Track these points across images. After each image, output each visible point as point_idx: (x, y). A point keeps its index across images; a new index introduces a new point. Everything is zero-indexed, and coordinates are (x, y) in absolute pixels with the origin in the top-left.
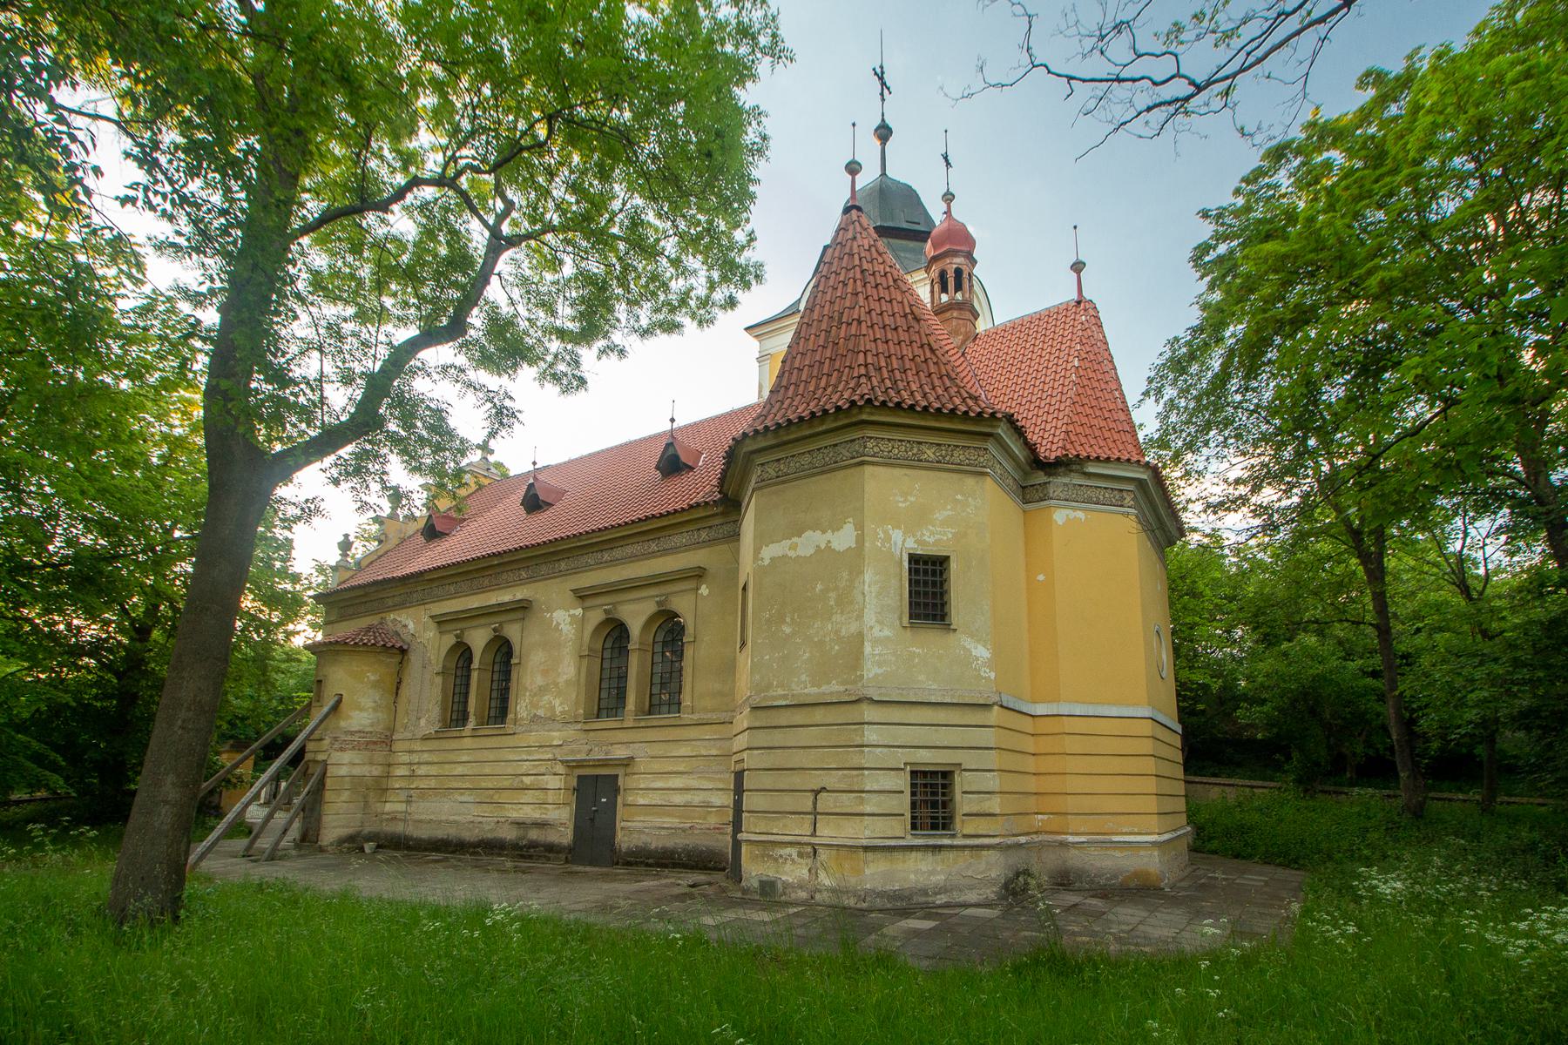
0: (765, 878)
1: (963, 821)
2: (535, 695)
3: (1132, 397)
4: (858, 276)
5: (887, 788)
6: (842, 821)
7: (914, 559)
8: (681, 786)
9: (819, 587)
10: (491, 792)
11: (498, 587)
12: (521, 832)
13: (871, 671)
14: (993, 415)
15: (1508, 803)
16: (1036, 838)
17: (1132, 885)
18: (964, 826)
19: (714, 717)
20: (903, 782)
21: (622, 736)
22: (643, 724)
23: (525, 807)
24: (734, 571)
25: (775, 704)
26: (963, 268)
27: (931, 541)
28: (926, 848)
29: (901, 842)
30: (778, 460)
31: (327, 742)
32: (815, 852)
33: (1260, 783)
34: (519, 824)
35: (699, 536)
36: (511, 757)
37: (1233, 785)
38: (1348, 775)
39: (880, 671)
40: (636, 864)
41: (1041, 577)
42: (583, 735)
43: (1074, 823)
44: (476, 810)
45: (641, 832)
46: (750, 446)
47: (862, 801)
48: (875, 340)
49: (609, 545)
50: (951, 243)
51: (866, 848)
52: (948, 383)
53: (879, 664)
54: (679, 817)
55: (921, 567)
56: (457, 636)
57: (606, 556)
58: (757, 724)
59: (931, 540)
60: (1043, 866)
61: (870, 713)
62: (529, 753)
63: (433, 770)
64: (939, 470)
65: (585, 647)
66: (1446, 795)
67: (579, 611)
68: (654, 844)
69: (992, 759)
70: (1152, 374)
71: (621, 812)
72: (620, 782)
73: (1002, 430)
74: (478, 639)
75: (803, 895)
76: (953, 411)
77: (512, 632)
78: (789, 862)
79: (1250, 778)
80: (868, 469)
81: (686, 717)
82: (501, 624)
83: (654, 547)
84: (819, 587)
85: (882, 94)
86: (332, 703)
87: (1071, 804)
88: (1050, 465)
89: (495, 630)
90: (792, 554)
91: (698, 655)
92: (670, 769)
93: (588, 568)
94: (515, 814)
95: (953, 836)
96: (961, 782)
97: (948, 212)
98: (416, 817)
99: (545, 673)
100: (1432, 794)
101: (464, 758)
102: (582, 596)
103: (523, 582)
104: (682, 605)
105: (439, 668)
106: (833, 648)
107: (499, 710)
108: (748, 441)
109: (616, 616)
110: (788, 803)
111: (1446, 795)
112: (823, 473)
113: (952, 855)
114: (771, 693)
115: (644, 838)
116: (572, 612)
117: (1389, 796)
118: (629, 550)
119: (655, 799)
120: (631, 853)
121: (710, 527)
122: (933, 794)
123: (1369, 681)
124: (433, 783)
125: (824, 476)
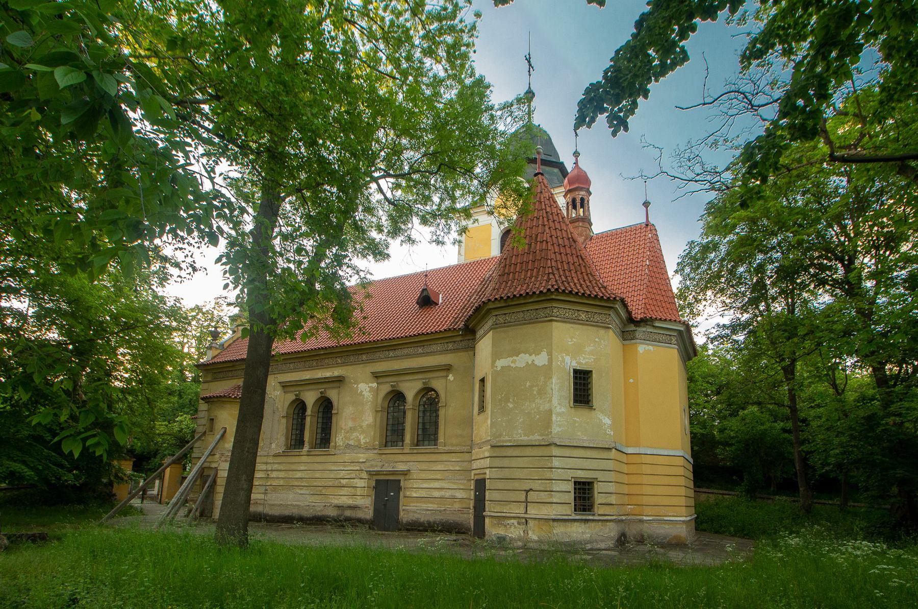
1: (598, 508)
2: (348, 432)
3: (670, 273)
4: (545, 215)
5: (564, 490)
6: (541, 506)
7: (576, 371)
9: (528, 384)
10: (320, 488)
12: (340, 512)
13: (555, 429)
14: (615, 298)
15: (854, 506)
16: (629, 518)
17: (673, 542)
18: (599, 510)
19: (458, 449)
20: (570, 487)
21: (402, 457)
22: (415, 451)
23: (342, 497)
24: (471, 367)
25: (505, 444)
26: (585, 197)
27: (584, 363)
28: (582, 520)
29: (570, 517)
30: (505, 314)
31: (217, 456)
32: (527, 521)
33: (727, 492)
34: (338, 507)
35: (448, 346)
37: (713, 493)
38: (772, 489)
39: (560, 430)
40: (412, 530)
41: (631, 381)
42: (377, 456)
43: (647, 510)
44: (313, 499)
46: (491, 306)
47: (551, 496)
48: (555, 253)
49: (394, 347)
50: (579, 183)
51: (554, 520)
52: (591, 279)
53: (560, 426)
54: (437, 504)
55: (578, 375)
56: (296, 395)
57: (391, 354)
58: (494, 455)
59: (584, 362)
60: (632, 531)
61: (555, 451)
63: (282, 475)
64: (587, 325)
65: (379, 406)
66: (823, 501)
67: (375, 385)
68: (423, 519)
69: (612, 476)
70: (680, 260)
71: (402, 500)
72: (402, 484)
73: (618, 306)
74: (310, 398)
75: (520, 544)
76: (596, 296)
77: (333, 394)
79: (721, 489)
80: (554, 324)
81: (441, 448)
82: (325, 389)
83: (420, 350)
84: (528, 384)
85: (529, 71)
86: (221, 433)
87: (646, 500)
88: (637, 321)
89: (321, 393)
90: (513, 365)
91: (448, 414)
92: (432, 477)
93: (380, 360)
94: (336, 501)
95: (594, 515)
96: (597, 488)
97: (576, 163)
98: (270, 502)
99: (354, 420)
100: (815, 501)
101: (302, 468)
102: (377, 376)
103: (338, 365)
104: (437, 384)
105: (284, 414)
106: (535, 417)
107: (324, 439)
108: (490, 303)
109: (398, 389)
110: (512, 496)
111: (823, 501)
112: (530, 323)
113: (593, 524)
114: (502, 439)
116: (370, 385)
117: (794, 501)
118: (405, 351)
119: (423, 493)
120: (408, 524)
121: (454, 342)
122: (584, 493)
123: (786, 435)
124: (282, 482)
125: (530, 325)
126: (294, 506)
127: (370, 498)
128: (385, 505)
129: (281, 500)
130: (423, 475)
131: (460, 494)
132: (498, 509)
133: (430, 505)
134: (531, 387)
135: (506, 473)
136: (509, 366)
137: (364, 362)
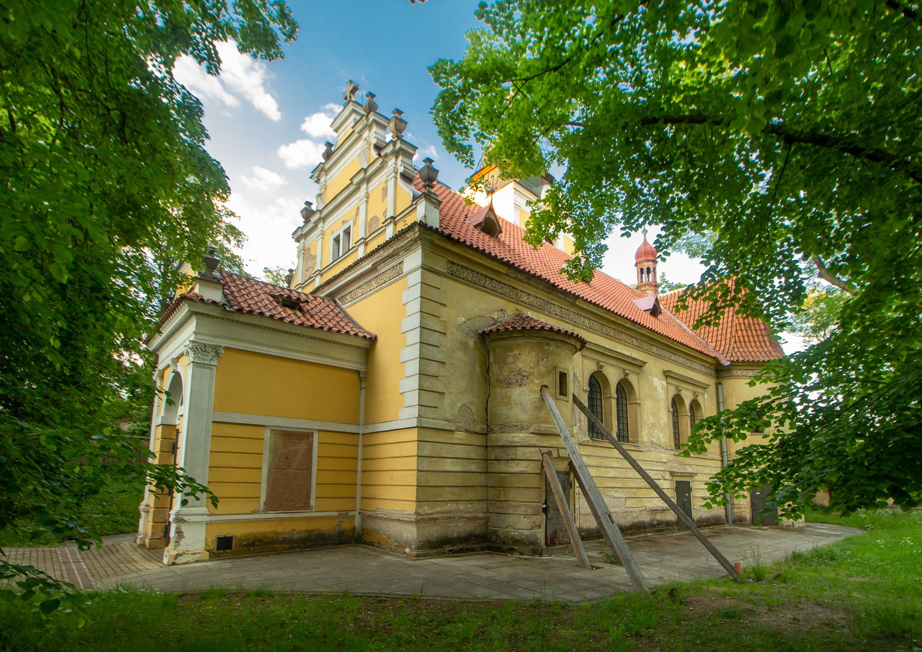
11: (620, 341)
42: (674, 458)
101: (615, 465)
118: (681, 360)
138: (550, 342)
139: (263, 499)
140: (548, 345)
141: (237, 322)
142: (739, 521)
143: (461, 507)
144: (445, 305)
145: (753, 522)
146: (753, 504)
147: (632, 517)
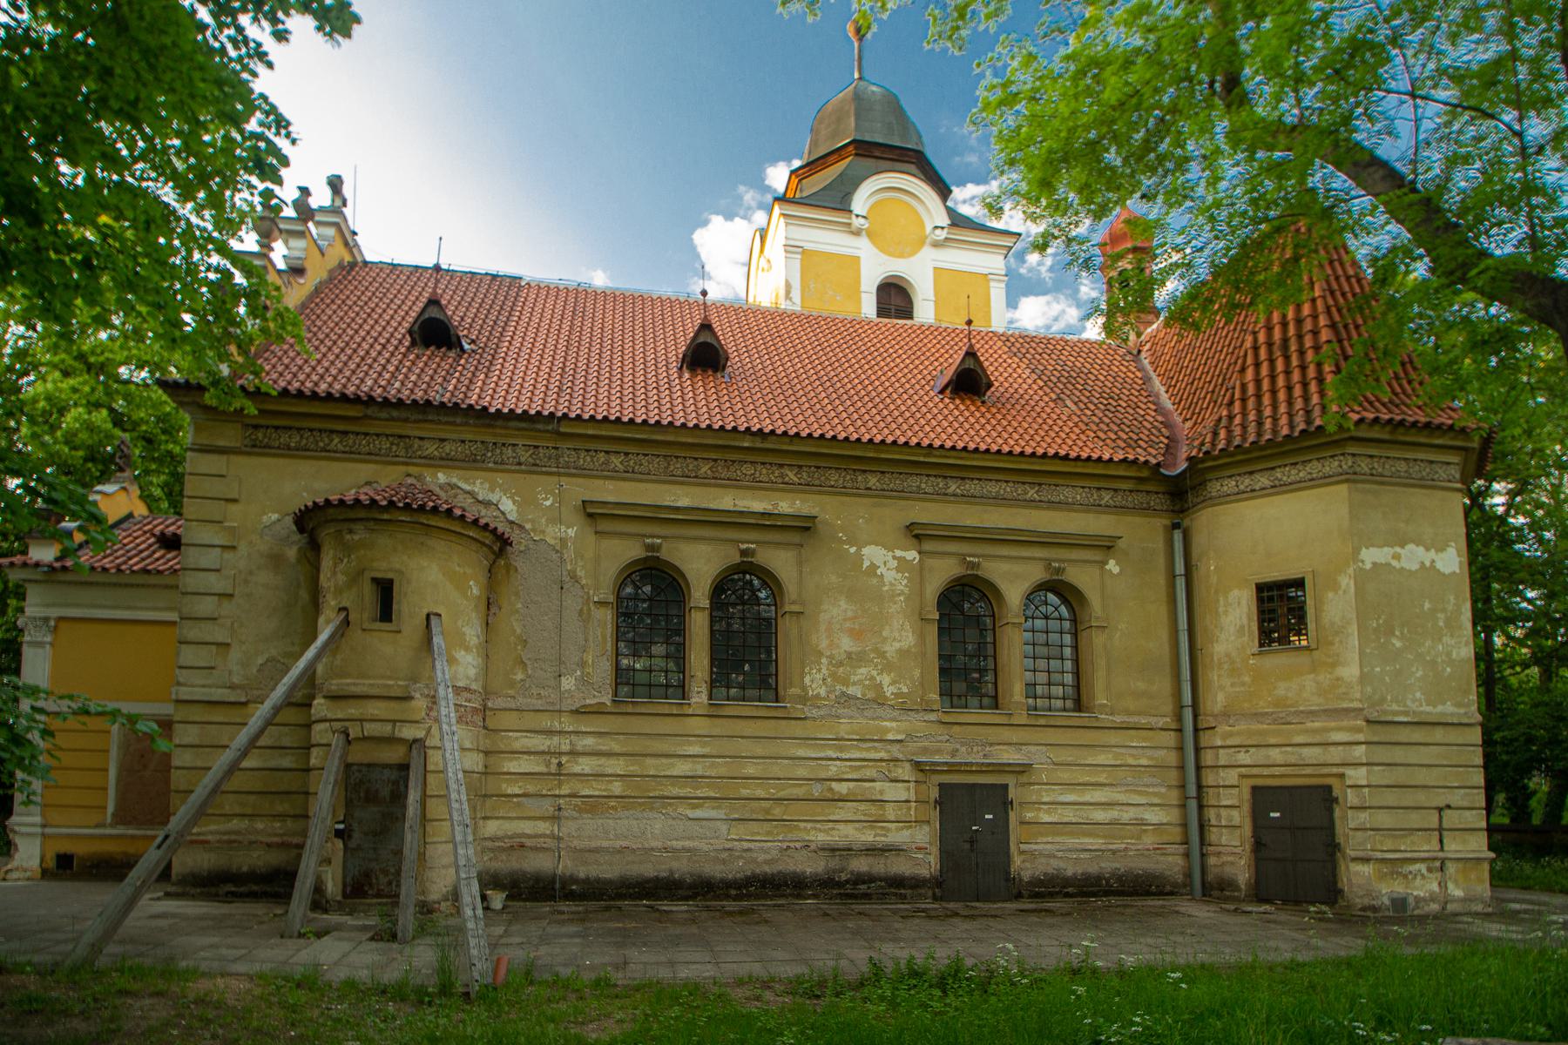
0: (1395, 895)
2: (841, 664)
6: (1467, 836)
8: (1103, 800)
9: (1427, 606)
10: (765, 804)
11: (734, 483)
21: (1006, 734)
22: (1042, 721)
23: (841, 826)
25: (1397, 719)
36: (801, 753)
42: (941, 729)
44: (738, 831)
45: (1051, 856)
54: (1104, 837)
57: (953, 487)
58: (1375, 739)
62: (841, 749)
67: (912, 555)
78: (1419, 877)
83: (1032, 493)
89: (744, 553)
90: (1394, 563)
92: (1087, 779)
99: (856, 635)
101: (695, 749)
110: (1415, 820)
115: (1055, 863)
116: (899, 553)
118: (993, 488)
119: (1069, 815)
120: (1036, 882)
121: (1116, 490)
124: (617, 788)
125: (1423, 491)
126: (675, 850)
127: (926, 828)
128: (972, 842)
129: (617, 837)
130: (1065, 775)
131: (1154, 816)
132: (1389, 845)
133: (1086, 840)
134: (1434, 610)
135: (1399, 776)
136: (1388, 565)
137: (883, 494)
138: (352, 526)
139: (111, 809)
140: (351, 531)
141: (64, 582)
142: (1215, 890)
143: (260, 825)
144: (235, 501)
145: (1260, 894)
146: (1258, 845)
147: (754, 861)
